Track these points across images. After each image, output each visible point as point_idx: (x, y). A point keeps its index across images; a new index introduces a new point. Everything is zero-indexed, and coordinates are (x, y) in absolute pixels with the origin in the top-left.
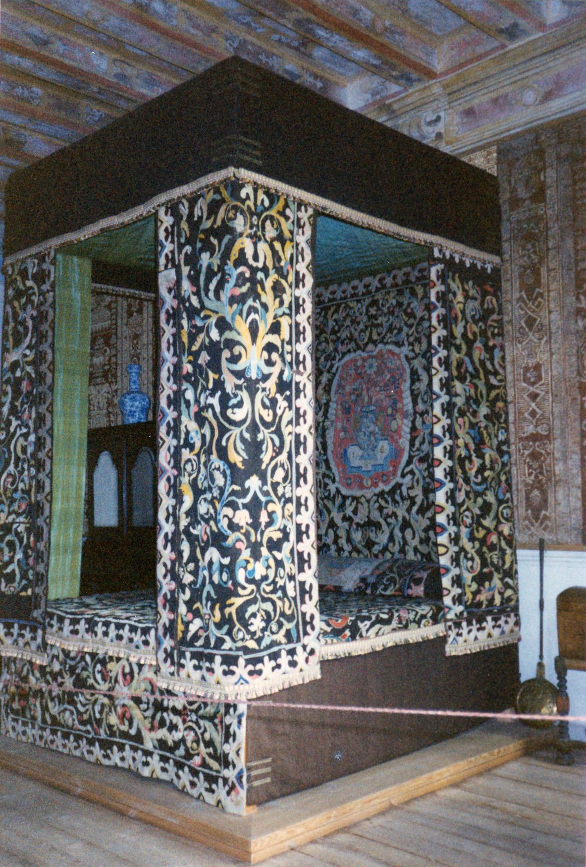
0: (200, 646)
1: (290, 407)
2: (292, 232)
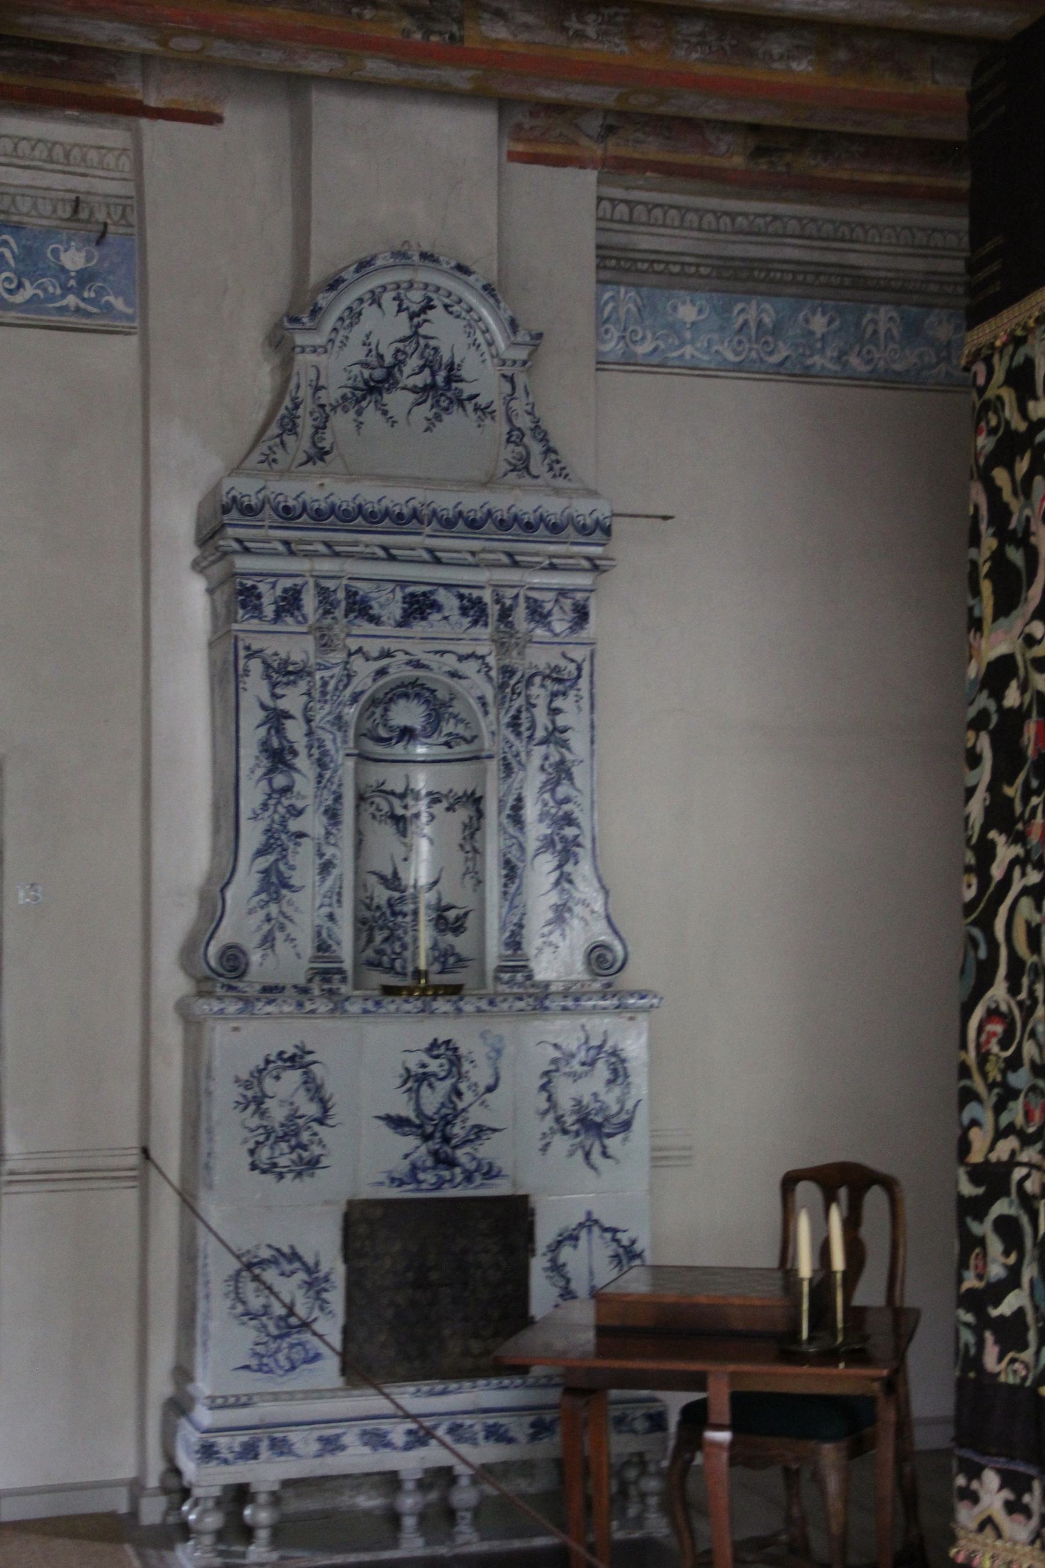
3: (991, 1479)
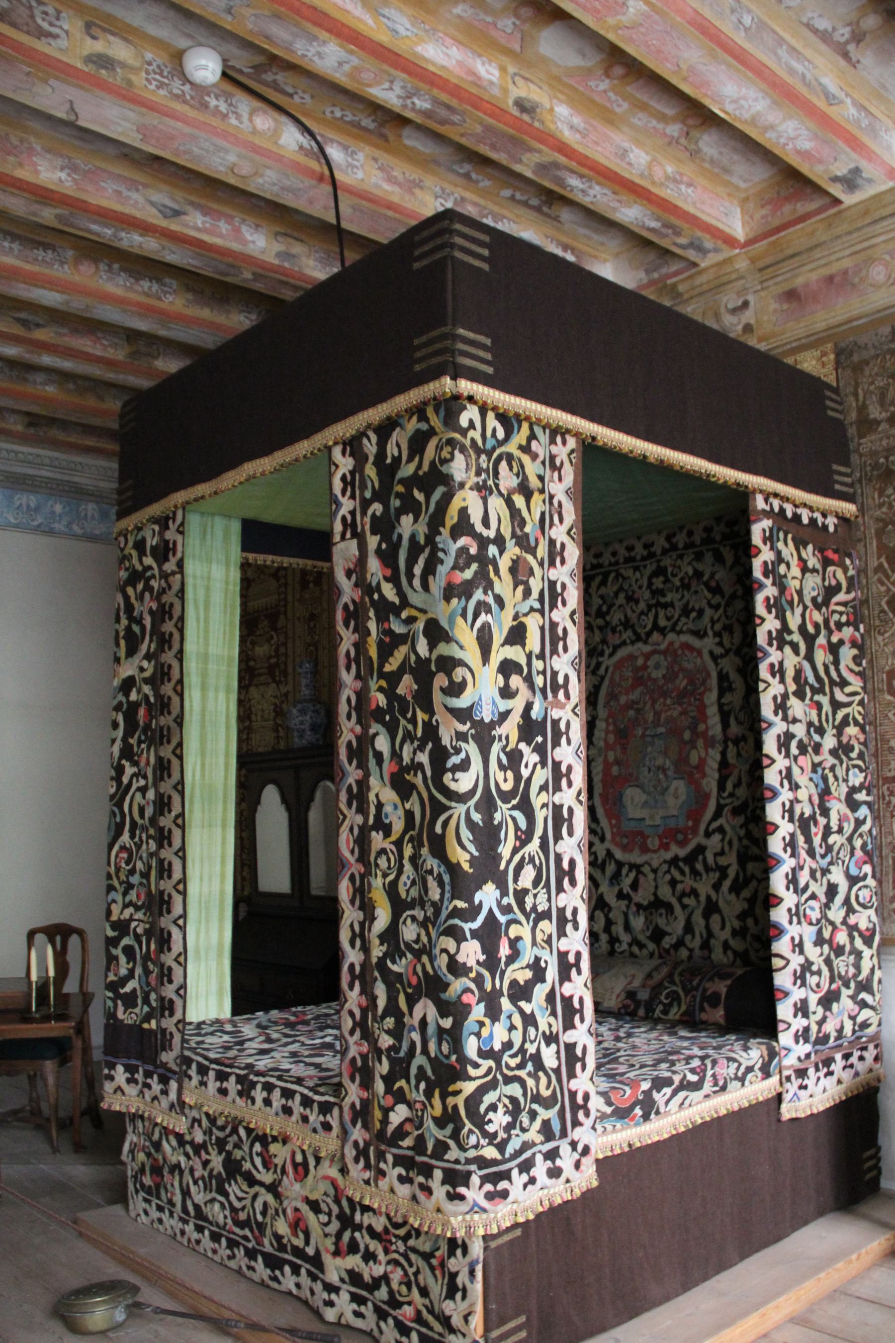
0: (408, 1148)
1: (544, 763)
2: (541, 478)
3: (120, 1069)
